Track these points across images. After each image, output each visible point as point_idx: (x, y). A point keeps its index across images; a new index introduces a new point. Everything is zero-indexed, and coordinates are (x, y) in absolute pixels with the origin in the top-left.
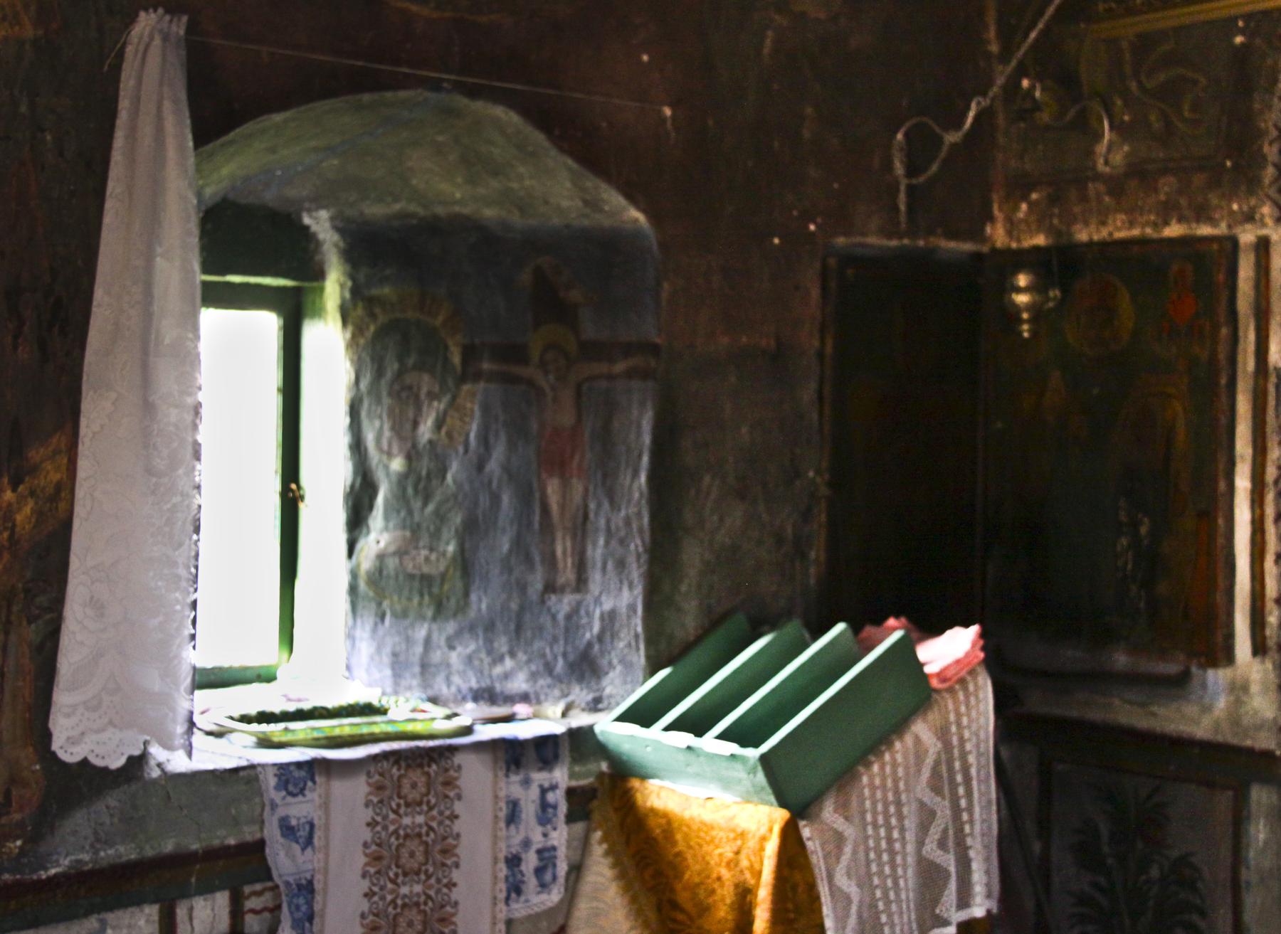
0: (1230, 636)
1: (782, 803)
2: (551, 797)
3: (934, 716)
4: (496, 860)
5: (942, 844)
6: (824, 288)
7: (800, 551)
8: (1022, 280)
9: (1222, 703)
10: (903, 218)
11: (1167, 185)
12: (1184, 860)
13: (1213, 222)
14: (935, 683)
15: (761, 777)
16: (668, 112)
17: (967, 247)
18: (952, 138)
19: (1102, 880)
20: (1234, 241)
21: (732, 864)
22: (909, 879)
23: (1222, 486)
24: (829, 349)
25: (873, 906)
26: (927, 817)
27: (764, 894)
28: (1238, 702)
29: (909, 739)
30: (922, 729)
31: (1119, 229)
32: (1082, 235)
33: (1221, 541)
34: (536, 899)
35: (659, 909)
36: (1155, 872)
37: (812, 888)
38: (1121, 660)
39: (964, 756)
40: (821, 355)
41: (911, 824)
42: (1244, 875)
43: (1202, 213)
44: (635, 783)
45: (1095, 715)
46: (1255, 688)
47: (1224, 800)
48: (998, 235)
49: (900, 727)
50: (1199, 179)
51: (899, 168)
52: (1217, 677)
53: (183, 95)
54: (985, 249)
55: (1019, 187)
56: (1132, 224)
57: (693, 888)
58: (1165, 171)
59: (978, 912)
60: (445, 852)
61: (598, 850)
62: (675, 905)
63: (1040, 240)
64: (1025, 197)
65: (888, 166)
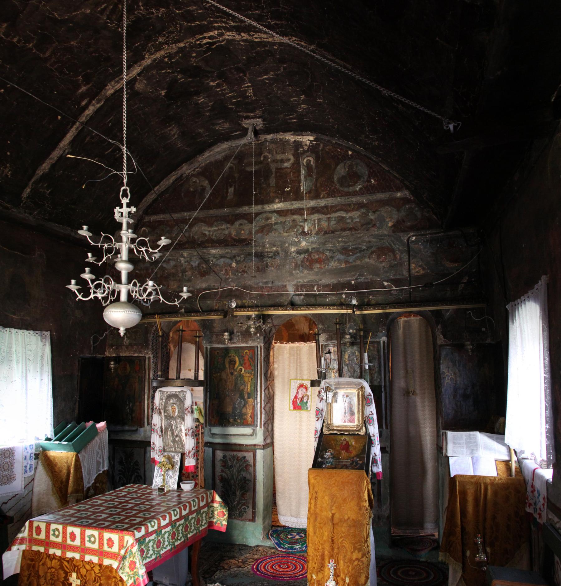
0: (144, 422)
1: (76, 452)
2: (32, 455)
3: (99, 436)
4: (22, 467)
5: (100, 458)
6: (79, 363)
7: (74, 411)
8: (112, 363)
9: (142, 434)
10: (92, 351)
11: (135, 347)
12: (136, 461)
13: (142, 354)
14: (99, 431)
15: (72, 447)
16: (54, 333)
17: (102, 356)
18: (101, 338)
19: (123, 467)
20: (145, 357)
21: (67, 463)
22: (95, 464)
23: (143, 397)
24: (79, 374)
25: (89, 468)
26: (98, 453)
27: (72, 466)
28: (145, 433)
29: (95, 440)
30: (97, 439)
31: (127, 354)
32: (121, 355)
33: (143, 407)
34: (29, 474)
35: (52, 473)
36: (132, 464)
37: (80, 465)
38: (127, 428)
39: (104, 443)
40: (78, 375)
41: (95, 454)
42: (146, 462)
43: (140, 352)
44: (47, 452)
45: (122, 438)
46: (148, 431)
47: (143, 450)
48: (107, 354)
49: (93, 438)
50: (140, 347)
51: (92, 343)
52: (142, 429)
53: (50, 344)
54: (105, 356)
55: (112, 346)
56: (129, 353)
57: (59, 468)
58: (134, 345)
59: (106, 469)
60: (12, 466)
61: (40, 464)
62: (55, 472)
63: (114, 355)
64: (112, 348)
65: (90, 342)
